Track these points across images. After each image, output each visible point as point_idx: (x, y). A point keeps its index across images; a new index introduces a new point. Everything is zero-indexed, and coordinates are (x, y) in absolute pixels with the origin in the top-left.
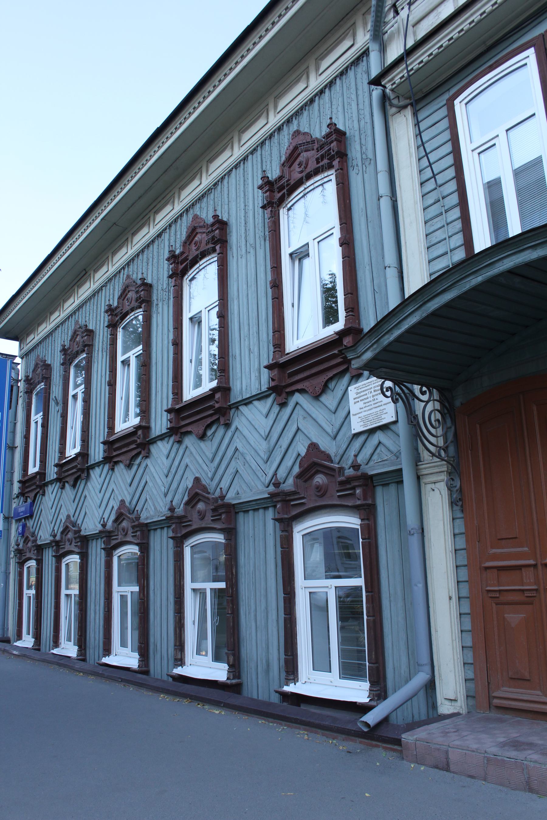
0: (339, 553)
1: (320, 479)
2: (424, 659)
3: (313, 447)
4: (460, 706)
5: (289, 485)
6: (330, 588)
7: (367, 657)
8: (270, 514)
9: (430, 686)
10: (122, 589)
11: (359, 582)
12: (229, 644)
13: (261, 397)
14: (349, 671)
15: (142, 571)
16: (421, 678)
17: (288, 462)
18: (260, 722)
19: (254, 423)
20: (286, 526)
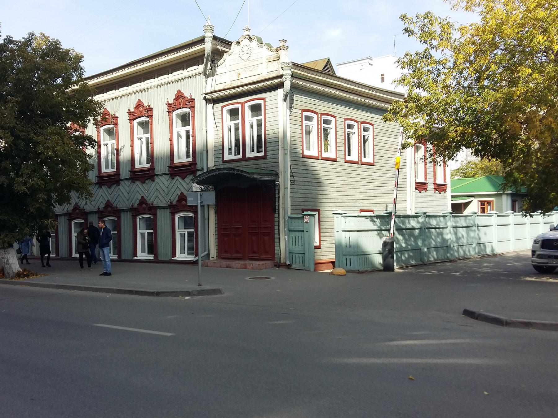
0: (187, 223)
1: (144, 206)
2: (207, 248)
3: (182, 193)
4: (215, 258)
5: (174, 203)
6: (146, 232)
7: (193, 250)
8: (168, 210)
9: (208, 255)
10: (141, 231)
11: (193, 230)
12: (152, 249)
13: (166, 174)
14: (150, 253)
15: (151, 224)
16: (206, 253)
17: (174, 195)
18: (247, 278)
19: (163, 182)
20: (70, 221)
